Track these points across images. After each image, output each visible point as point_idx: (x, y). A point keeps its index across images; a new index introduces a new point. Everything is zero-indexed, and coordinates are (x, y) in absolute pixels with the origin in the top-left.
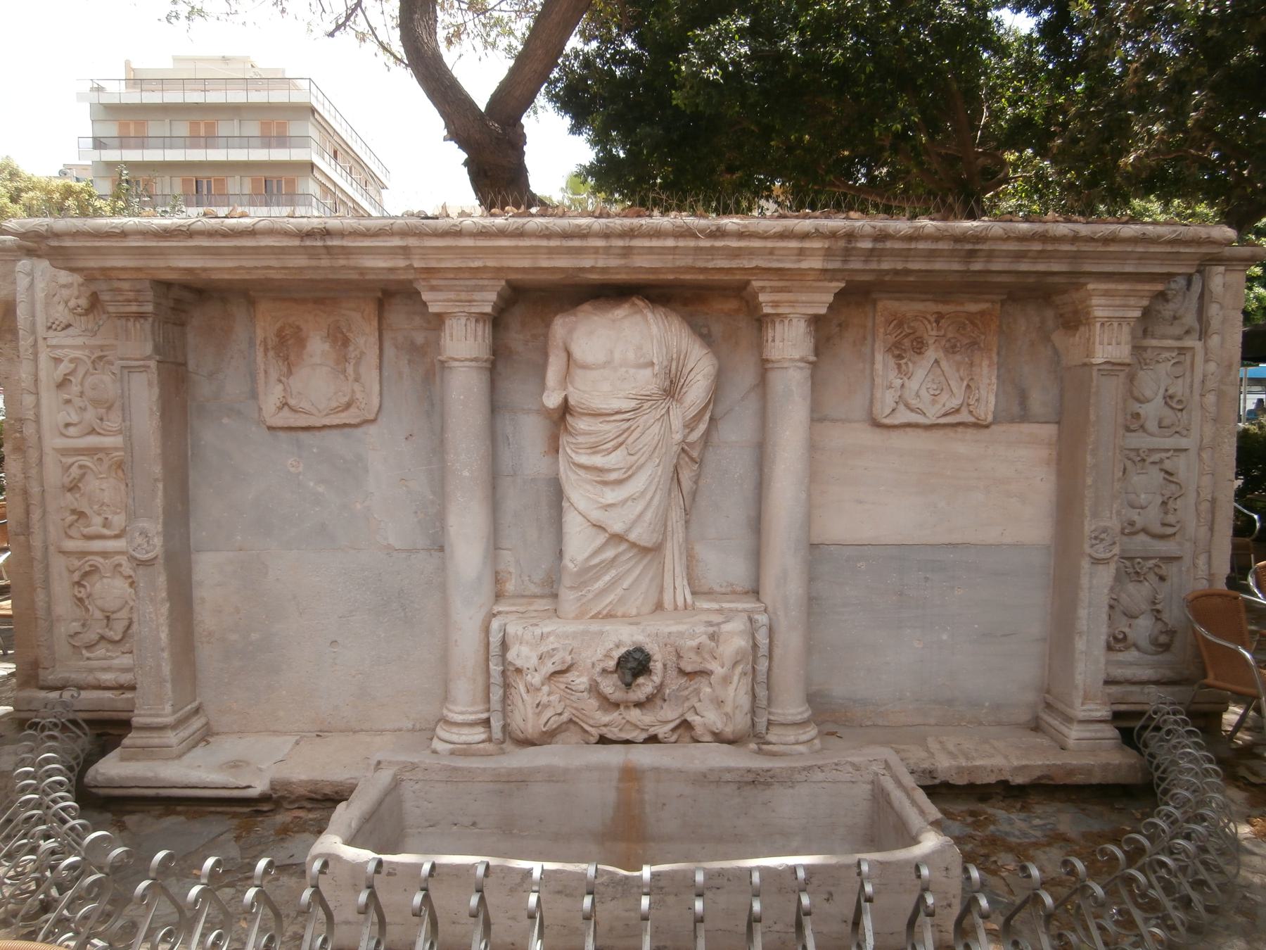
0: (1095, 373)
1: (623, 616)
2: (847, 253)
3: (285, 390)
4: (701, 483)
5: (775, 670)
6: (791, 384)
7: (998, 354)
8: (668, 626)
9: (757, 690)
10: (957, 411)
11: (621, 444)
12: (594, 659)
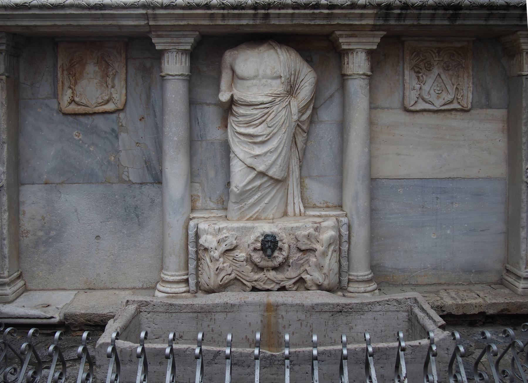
0: (524, 80)
1: (265, 219)
2: (386, 17)
3: (73, 93)
4: (309, 144)
5: (352, 250)
6: (357, 88)
7: (473, 70)
8: (290, 223)
9: (342, 261)
10: (451, 102)
11: (264, 121)
12: (249, 242)
